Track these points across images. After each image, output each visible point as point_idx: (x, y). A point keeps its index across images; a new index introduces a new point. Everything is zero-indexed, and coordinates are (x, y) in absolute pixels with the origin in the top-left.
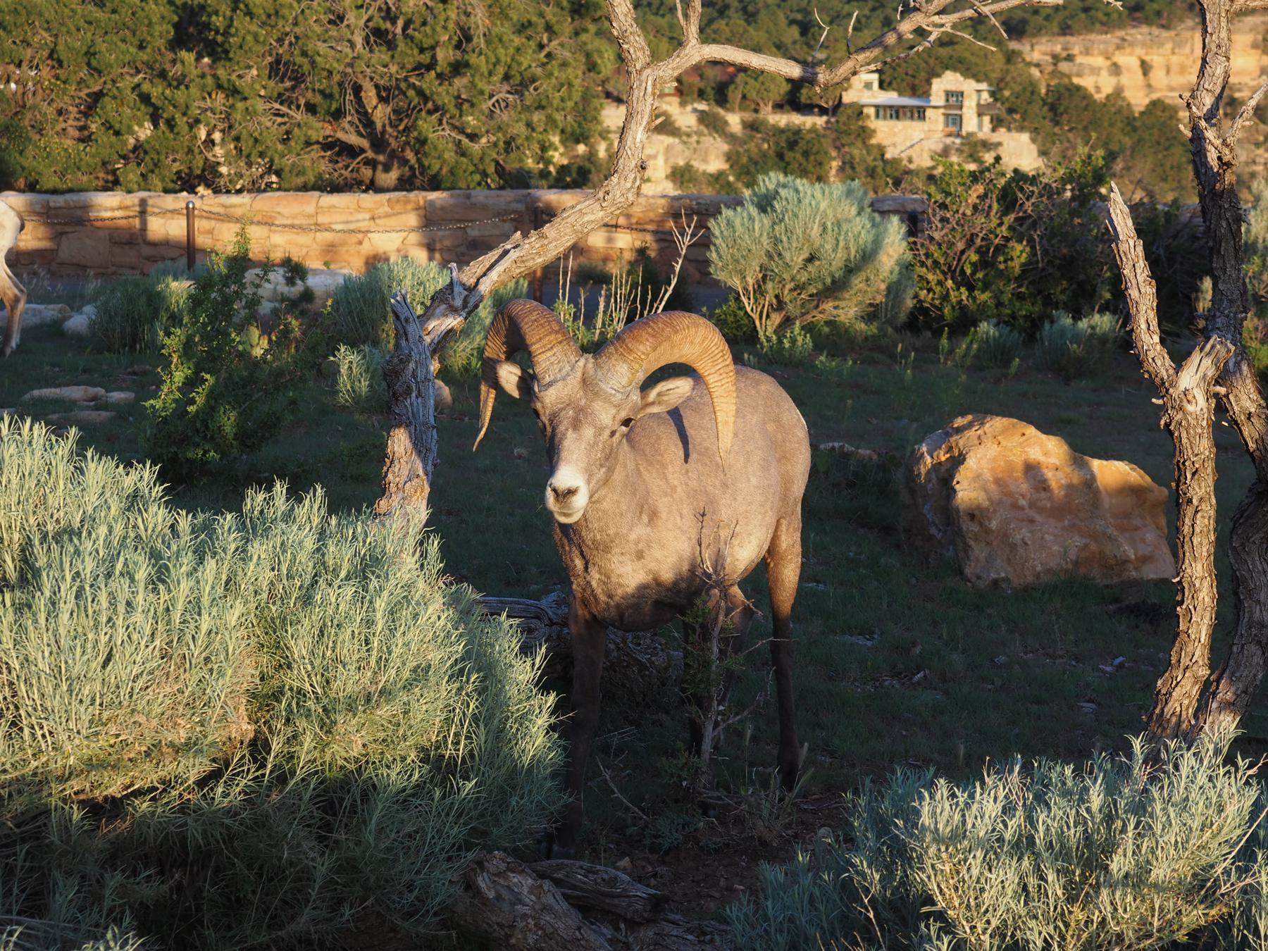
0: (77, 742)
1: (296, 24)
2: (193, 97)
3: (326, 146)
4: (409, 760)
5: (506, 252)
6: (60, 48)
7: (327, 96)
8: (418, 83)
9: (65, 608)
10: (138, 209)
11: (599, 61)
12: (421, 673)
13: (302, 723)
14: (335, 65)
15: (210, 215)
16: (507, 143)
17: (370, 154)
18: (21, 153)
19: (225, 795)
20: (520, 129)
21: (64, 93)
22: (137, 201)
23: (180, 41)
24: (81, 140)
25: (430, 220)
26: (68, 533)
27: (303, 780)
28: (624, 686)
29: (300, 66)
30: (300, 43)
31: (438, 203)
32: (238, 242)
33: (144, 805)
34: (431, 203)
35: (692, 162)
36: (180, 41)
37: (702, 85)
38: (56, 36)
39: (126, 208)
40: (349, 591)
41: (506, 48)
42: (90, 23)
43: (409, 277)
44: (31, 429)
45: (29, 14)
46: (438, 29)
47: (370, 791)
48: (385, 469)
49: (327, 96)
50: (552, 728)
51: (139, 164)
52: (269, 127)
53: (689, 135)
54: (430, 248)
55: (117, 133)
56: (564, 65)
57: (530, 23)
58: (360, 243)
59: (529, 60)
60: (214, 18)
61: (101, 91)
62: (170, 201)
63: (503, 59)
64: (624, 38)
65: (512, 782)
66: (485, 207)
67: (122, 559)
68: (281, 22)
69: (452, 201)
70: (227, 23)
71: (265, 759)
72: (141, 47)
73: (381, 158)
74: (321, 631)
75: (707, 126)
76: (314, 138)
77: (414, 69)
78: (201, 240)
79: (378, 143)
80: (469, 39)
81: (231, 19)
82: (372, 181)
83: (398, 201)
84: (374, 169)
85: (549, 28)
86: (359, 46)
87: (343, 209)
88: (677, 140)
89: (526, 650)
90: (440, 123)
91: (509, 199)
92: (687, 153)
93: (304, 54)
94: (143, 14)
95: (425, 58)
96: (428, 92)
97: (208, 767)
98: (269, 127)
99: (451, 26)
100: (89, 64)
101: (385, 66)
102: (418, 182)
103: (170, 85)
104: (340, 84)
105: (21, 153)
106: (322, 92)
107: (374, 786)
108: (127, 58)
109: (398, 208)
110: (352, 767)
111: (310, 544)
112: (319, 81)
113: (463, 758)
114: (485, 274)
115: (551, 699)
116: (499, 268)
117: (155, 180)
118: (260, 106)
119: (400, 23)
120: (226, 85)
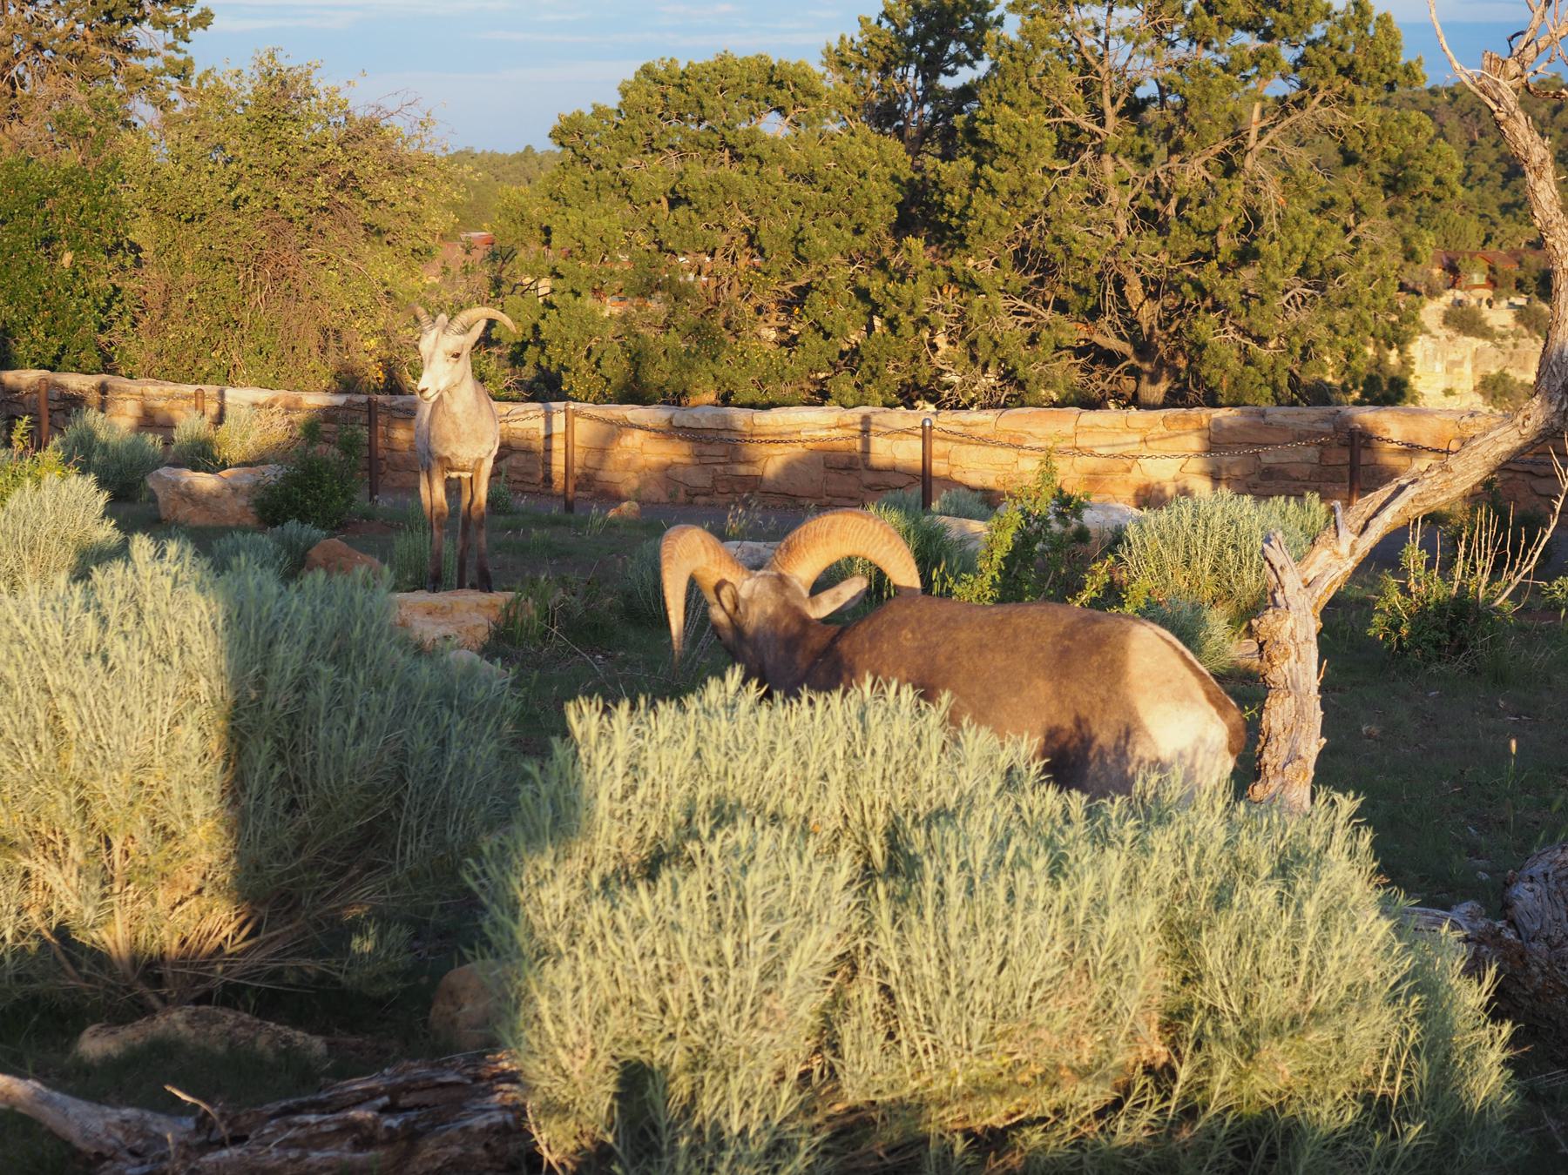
0: (966, 1060)
1: (1046, 203)
2: (919, 292)
3: (1079, 352)
4: (1339, 1096)
5: (1401, 489)
6: (762, 233)
7: (1082, 291)
8: (1193, 275)
9: (955, 899)
10: (859, 427)
11: (1419, 248)
12: (1357, 994)
13: (1217, 1051)
14: (1096, 253)
15: (948, 436)
16: (1305, 349)
17: (1133, 360)
18: (714, 359)
19: (1128, 1129)
20: (1320, 331)
21: (765, 288)
22: (858, 419)
23: (903, 226)
24: (782, 344)
25: (1216, 443)
26: (941, 815)
27: (1217, 1116)
28: (1549, 1018)
29: (1052, 255)
30: (1052, 226)
31: (1226, 422)
32: (1042, 472)
33: (1035, 1137)
34: (1217, 422)
35: (1508, 371)
36: (903, 226)
37: (1521, 274)
38: (757, 219)
39: (846, 426)
40: (1271, 893)
41: (1305, 233)
42: (798, 203)
43: (1219, 514)
44: (898, 693)
45: (726, 192)
46: (1221, 209)
47: (1292, 1132)
48: (1259, 747)
49: (1082, 291)
50: (1507, 1063)
51: (853, 373)
52: (1010, 329)
53: (1503, 337)
54: (1215, 478)
55: (827, 336)
56: (1375, 252)
57: (1333, 202)
58: (1129, 470)
59: (1333, 246)
60: (948, 197)
61: (808, 285)
62: (900, 417)
63: (1301, 246)
64: (1548, 229)
65: (1455, 1127)
66: (1283, 428)
67: (1012, 847)
68: (1029, 202)
69: (1242, 420)
70: (964, 202)
71: (1171, 1091)
72: (857, 231)
73: (1147, 367)
74: (1239, 939)
75: (1527, 326)
76: (1067, 343)
77: (1190, 259)
78: (939, 467)
79: (1144, 349)
80: (1258, 221)
81: (969, 198)
82: (1135, 394)
83: (1176, 419)
84: (1138, 380)
85: (1356, 208)
86: (1123, 231)
87: (1109, 428)
88: (1489, 343)
89: (1473, 969)
90: (1222, 321)
91: (1312, 418)
92: (1501, 359)
93: (1057, 240)
94: (862, 192)
95: (1204, 245)
96: (1207, 286)
97: (1111, 1095)
98: (1010, 329)
99: (1237, 205)
100: (796, 252)
101: (1155, 255)
102: (1191, 397)
103: (891, 278)
104: (1099, 276)
105: (714, 359)
106: (1076, 287)
107: (1298, 1125)
108: (842, 246)
109: (1176, 429)
110: (1274, 1102)
111: (1221, 835)
112: (1074, 273)
113: (1400, 1097)
114: (1375, 515)
115: (1507, 1029)
116: (1394, 507)
117: (872, 391)
118: (1001, 303)
119: (1173, 203)
120: (961, 278)
